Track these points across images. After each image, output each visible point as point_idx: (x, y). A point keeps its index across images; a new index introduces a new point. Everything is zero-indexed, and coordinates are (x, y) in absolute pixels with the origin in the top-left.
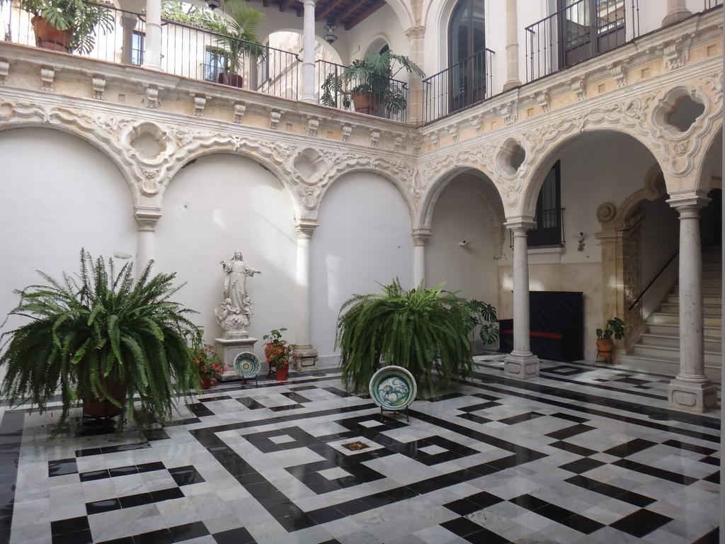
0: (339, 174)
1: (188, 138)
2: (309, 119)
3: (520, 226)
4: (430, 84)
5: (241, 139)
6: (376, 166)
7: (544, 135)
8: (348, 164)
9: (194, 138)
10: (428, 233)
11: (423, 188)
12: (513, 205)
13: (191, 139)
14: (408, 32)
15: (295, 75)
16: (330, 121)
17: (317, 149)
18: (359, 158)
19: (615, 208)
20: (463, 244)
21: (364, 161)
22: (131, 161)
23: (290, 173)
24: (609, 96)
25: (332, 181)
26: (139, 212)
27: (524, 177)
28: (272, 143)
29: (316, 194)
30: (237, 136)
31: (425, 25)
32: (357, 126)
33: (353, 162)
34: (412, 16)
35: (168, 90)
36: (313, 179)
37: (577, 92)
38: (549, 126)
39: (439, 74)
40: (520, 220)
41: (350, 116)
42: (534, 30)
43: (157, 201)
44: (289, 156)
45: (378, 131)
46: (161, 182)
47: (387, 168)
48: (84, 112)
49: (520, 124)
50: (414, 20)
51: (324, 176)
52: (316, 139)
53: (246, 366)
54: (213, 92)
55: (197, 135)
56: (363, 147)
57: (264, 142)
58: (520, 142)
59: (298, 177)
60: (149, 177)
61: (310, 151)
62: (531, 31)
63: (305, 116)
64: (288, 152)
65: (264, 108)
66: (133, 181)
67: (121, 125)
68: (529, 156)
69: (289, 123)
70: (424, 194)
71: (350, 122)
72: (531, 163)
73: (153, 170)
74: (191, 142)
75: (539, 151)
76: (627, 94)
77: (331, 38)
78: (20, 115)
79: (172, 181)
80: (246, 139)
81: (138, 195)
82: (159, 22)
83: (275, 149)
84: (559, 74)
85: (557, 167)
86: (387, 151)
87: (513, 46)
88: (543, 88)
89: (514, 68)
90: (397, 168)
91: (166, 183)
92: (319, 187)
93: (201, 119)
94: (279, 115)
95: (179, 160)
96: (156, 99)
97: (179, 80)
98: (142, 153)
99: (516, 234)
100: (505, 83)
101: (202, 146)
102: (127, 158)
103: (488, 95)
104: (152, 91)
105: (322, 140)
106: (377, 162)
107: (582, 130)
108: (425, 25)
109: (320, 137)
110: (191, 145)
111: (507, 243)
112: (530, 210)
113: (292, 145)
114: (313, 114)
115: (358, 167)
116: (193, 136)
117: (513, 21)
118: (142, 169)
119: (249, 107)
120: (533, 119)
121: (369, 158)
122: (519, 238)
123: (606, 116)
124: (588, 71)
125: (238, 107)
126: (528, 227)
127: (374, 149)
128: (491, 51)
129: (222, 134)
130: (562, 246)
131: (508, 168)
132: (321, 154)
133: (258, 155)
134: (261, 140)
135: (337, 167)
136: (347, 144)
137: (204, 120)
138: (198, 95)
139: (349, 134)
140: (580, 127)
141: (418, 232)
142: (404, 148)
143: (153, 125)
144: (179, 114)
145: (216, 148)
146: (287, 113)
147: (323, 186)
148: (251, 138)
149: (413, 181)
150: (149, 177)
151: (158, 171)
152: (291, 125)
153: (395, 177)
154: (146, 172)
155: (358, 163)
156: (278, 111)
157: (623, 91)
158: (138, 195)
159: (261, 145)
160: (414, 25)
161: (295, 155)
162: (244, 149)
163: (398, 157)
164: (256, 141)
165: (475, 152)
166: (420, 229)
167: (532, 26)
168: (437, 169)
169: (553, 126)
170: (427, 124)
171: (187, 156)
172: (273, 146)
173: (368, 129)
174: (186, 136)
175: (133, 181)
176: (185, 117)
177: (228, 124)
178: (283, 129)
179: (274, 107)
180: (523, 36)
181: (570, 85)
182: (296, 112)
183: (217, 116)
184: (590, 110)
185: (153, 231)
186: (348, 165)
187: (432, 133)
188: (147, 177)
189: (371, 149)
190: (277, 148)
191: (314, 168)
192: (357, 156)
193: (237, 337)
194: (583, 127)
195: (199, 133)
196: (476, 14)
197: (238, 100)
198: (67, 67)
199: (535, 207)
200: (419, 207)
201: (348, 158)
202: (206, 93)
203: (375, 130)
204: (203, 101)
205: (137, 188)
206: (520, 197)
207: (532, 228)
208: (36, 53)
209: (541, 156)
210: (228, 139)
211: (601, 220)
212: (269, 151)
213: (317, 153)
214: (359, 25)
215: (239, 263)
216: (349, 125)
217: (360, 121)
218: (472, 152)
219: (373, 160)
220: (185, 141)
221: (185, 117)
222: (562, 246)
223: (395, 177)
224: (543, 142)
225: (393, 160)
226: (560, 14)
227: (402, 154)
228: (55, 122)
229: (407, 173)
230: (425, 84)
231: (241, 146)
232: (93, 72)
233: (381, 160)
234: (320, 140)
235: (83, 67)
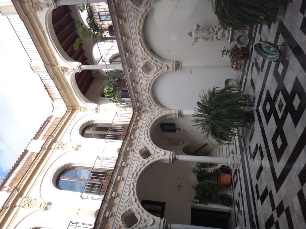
1: (143, 56)
9: (142, 54)
22: (157, 73)
23: (149, 160)
28: (134, 20)
30: (136, 37)
47: (137, 174)
48: (145, 86)
53: (243, 39)
54: (122, 51)
55: (141, 53)
57: (134, 24)
59: (147, 4)
60: (161, 68)
61: (141, 152)
64: (135, 11)
65: (120, 27)
67: (145, 76)
73: (159, 67)
78: (150, 99)
83: (136, 18)
97: (123, 65)
101: (145, 51)
104: (131, 71)
116: (142, 55)
129: (137, 43)
134: (134, 25)
137: (134, 51)
146: (117, 16)
150: (161, 68)
158: (168, 71)
162: (141, 33)
164: (135, 28)
172: (135, 20)
174: (142, 57)
175: (164, 72)
177: (132, 42)
182: (115, 12)
190: (135, 17)
193: (229, 36)
195: (140, 52)
197: (121, 41)
198: (133, 92)
208: (132, 99)
212: (138, 22)
215: (193, 34)
220: (145, 57)
228: (150, 92)
231: (140, 35)
232: (131, 86)
235: (131, 89)
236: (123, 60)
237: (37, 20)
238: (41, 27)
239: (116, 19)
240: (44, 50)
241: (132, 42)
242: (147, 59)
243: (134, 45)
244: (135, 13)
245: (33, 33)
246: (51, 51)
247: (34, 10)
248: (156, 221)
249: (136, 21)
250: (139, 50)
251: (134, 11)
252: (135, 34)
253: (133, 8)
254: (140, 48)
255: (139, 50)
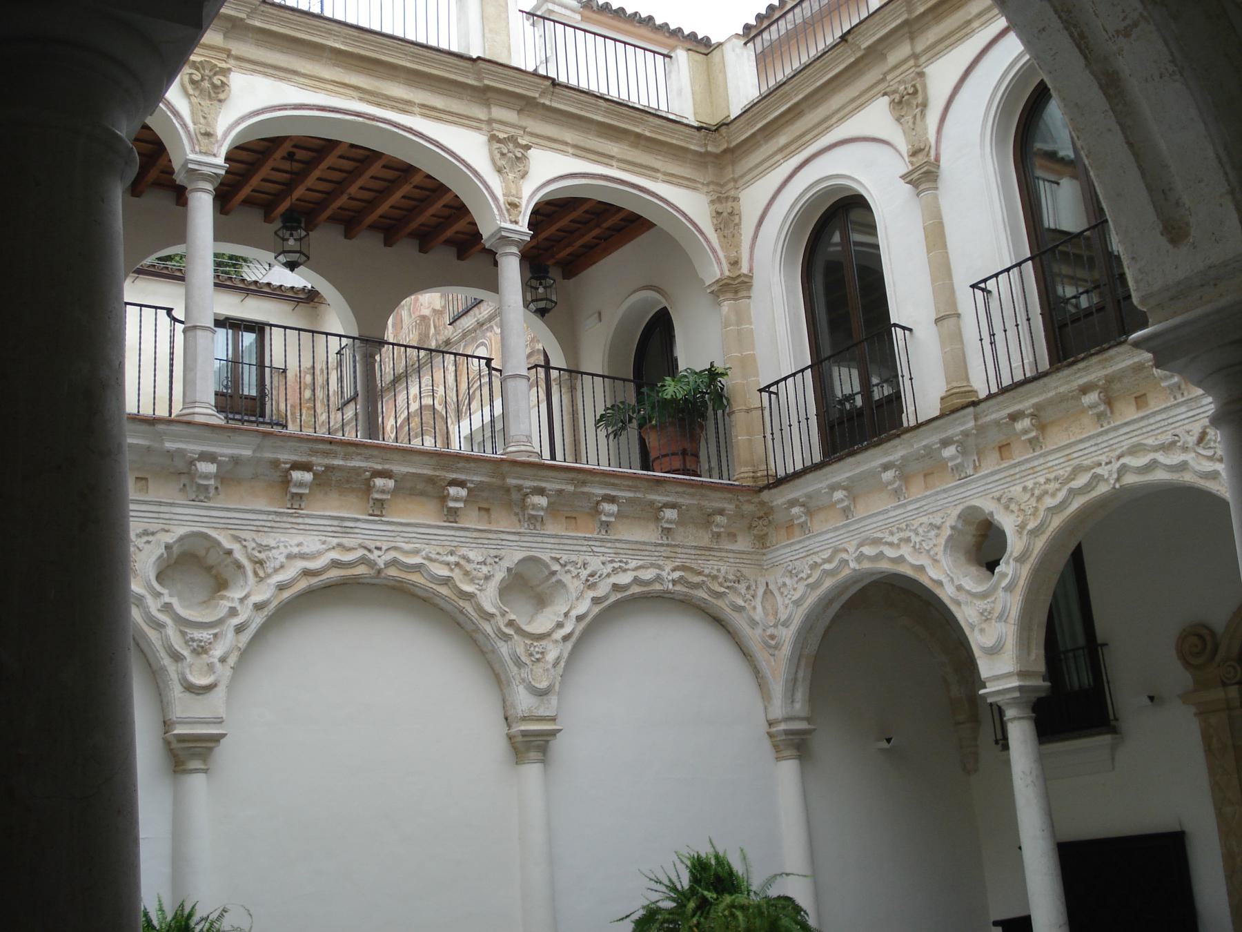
0: (596, 609)
2: (526, 495)
3: (1017, 694)
4: (777, 394)
5: (388, 550)
6: (674, 582)
7: (1039, 499)
8: (615, 585)
9: (290, 557)
10: (803, 725)
11: (783, 625)
12: (993, 651)
13: (282, 559)
14: (715, 288)
15: (438, 375)
16: (574, 494)
17: (545, 557)
18: (636, 569)
19: (1212, 633)
20: (885, 745)
21: (648, 575)
22: (162, 617)
23: (492, 615)
24: (1159, 418)
25: (583, 625)
26: (179, 730)
27: (1009, 588)
28: (452, 553)
29: (551, 656)
30: (378, 544)
31: (751, 270)
32: (629, 500)
33: (625, 579)
34: (721, 254)
35: (236, 460)
36: (541, 624)
37: (1095, 411)
38: (1048, 481)
39: (794, 375)
40: (1015, 683)
41: (612, 481)
42: (988, 288)
43: (215, 703)
44: (487, 578)
45: (673, 506)
46: (223, 660)
47: (697, 586)
49: (986, 476)
50: (724, 261)
51: (566, 615)
52: (543, 536)
55: (295, 550)
56: (644, 543)
57: (432, 551)
58: (992, 513)
59: (511, 623)
62: (983, 290)
63: (519, 488)
64: (485, 569)
65: (431, 480)
66: (167, 661)
68: (1015, 544)
69: (485, 506)
70: (787, 635)
71: (614, 493)
72: (1021, 559)
73: (205, 635)
74: (282, 567)
75: (1035, 533)
76: (1191, 414)
77: (542, 304)
79: (246, 654)
80: (395, 548)
81: (177, 691)
82: (211, 324)
83: (457, 564)
84: (1054, 377)
85: (1077, 557)
86: (696, 548)
87: (947, 317)
88: (1027, 403)
89: (957, 364)
90: (721, 585)
91: (232, 660)
92: (557, 641)
93: (301, 516)
94: (463, 493)
95: (259, 607)
96: (212, 482)
98: (180, 596)
99: (1010, 713)
100: (943, 394)
101: (307, 573)
102: (154, 612)
103: (909, 419)
105: (555, 536)
106: (676, 575)
107: (1117, 486)
108: (751, 270)
109: (551, 528)
110: (282, 571)
111: (987, 733)
112: (1033, 657)
113: (493, 553)
114: (535, 484)
115: (636, 589)
116: (286, 552)
117: (941, 270)
118: (183, 634)
119: (400, 480)
120: (1014, 466)
121: (660, 567)
122: (1016, 723)
123: (1161, 457)
124: (1109, 371)
125: (379, 482)
126: (1033, 697)
127: (668, 545)
128: (904, 328)
130: (1114, 730)
131: (974, 570)
132: (556, 567)
133: (422, 581)
135: (591, 594)
136: (610, 541)
137: (308, 516)
138: (296, 466)
139: (612, 519)
140: (1112, 482)
141: (783, 727)
142: (732, 536)
143: (206, 536)
144: (258, 508)
145: (334, 574)
146: (481, 487)
147: (566, 638)
148: (407, 547)
149: (759, 609)
151: (215, 635)
152: (487, 510)
153: (720, 603)
154: (193, 640)
155: (636, 581)
156: (461, 484)
157: (1183, 409)
159: (431, 560)
160: (727, 273)
161: (500, 575)
163: (721, 559)
164: (416, 552)
165: (895, 540)
166: (787, 719)
167: (985, 281)
168: (811, 580)
169: (1056, 479)
170: (780, 482)
171: (274, 596)
172: (452, 559)
173: (652, 503)
175: (167, 661)
176: (269, 513)
177: (357, 520)
178: (472, 520)
179: (454, 476)
180: (966, 301)
181: (1077, 398)
183: (334, 507)
184: (1126, 445)
185: (206, 771)
186: (616, 587)
187: (793, 503)
188: (194, 651)
189: (662, 545)
190: (462, 562)
191: (541, 601)
192: (633, 564)
194: (1118, 480)
196: (856, 237)
197: (379, 467)
199: (1042, 652)
200: (777, 668)
201: (614, 570)
202: (314, 459)
203: (667, 505)
204: (308, 477)
205: (174, 676)
206: (1007, 631)
207: (1043, 695)
209: (1040, 544)
210: (360, 553)
211: (1187, 665)
212: (443, 572)
213: (547, 566)
214: (594, 267)
216: (611, 499)
217: (629, 488)
218: (890, 539)
219: (668, 569)
220: (270, 566)
221: (269, 513)
222: (1114, 730)
223: (720, 603)
224: (1041, 514)
225: (711, 566)
226: (1037, 259)
227: (727, 551)
229: (743, 591)
230: (765, 395)
231: (387, 565)
233: (683, 568)
234: (550, 536)
236: (372, 456)
237: (952, 33)
238: (429, 111)
239: (475, 478)
240: (322, 47)
241: (357, 520)
242: (256, 574)
243: (336, 523)
244: (478, 563)
245: (410, 61)
246: (318, 82)
247: (502, 136)
248: (386, 548)
249: (448, 564)
250: (311, 543)
251: (484, 563)
252: (393, 544)
253: (497, 560)
254: (320, 553)
255: (311, 543)
